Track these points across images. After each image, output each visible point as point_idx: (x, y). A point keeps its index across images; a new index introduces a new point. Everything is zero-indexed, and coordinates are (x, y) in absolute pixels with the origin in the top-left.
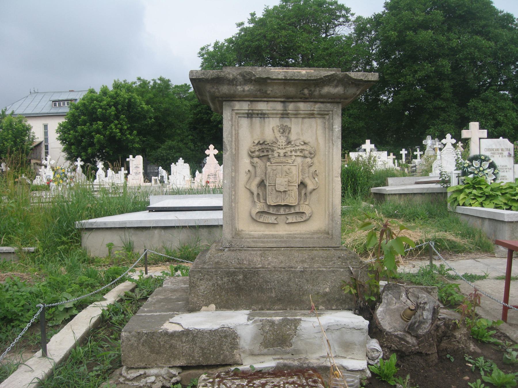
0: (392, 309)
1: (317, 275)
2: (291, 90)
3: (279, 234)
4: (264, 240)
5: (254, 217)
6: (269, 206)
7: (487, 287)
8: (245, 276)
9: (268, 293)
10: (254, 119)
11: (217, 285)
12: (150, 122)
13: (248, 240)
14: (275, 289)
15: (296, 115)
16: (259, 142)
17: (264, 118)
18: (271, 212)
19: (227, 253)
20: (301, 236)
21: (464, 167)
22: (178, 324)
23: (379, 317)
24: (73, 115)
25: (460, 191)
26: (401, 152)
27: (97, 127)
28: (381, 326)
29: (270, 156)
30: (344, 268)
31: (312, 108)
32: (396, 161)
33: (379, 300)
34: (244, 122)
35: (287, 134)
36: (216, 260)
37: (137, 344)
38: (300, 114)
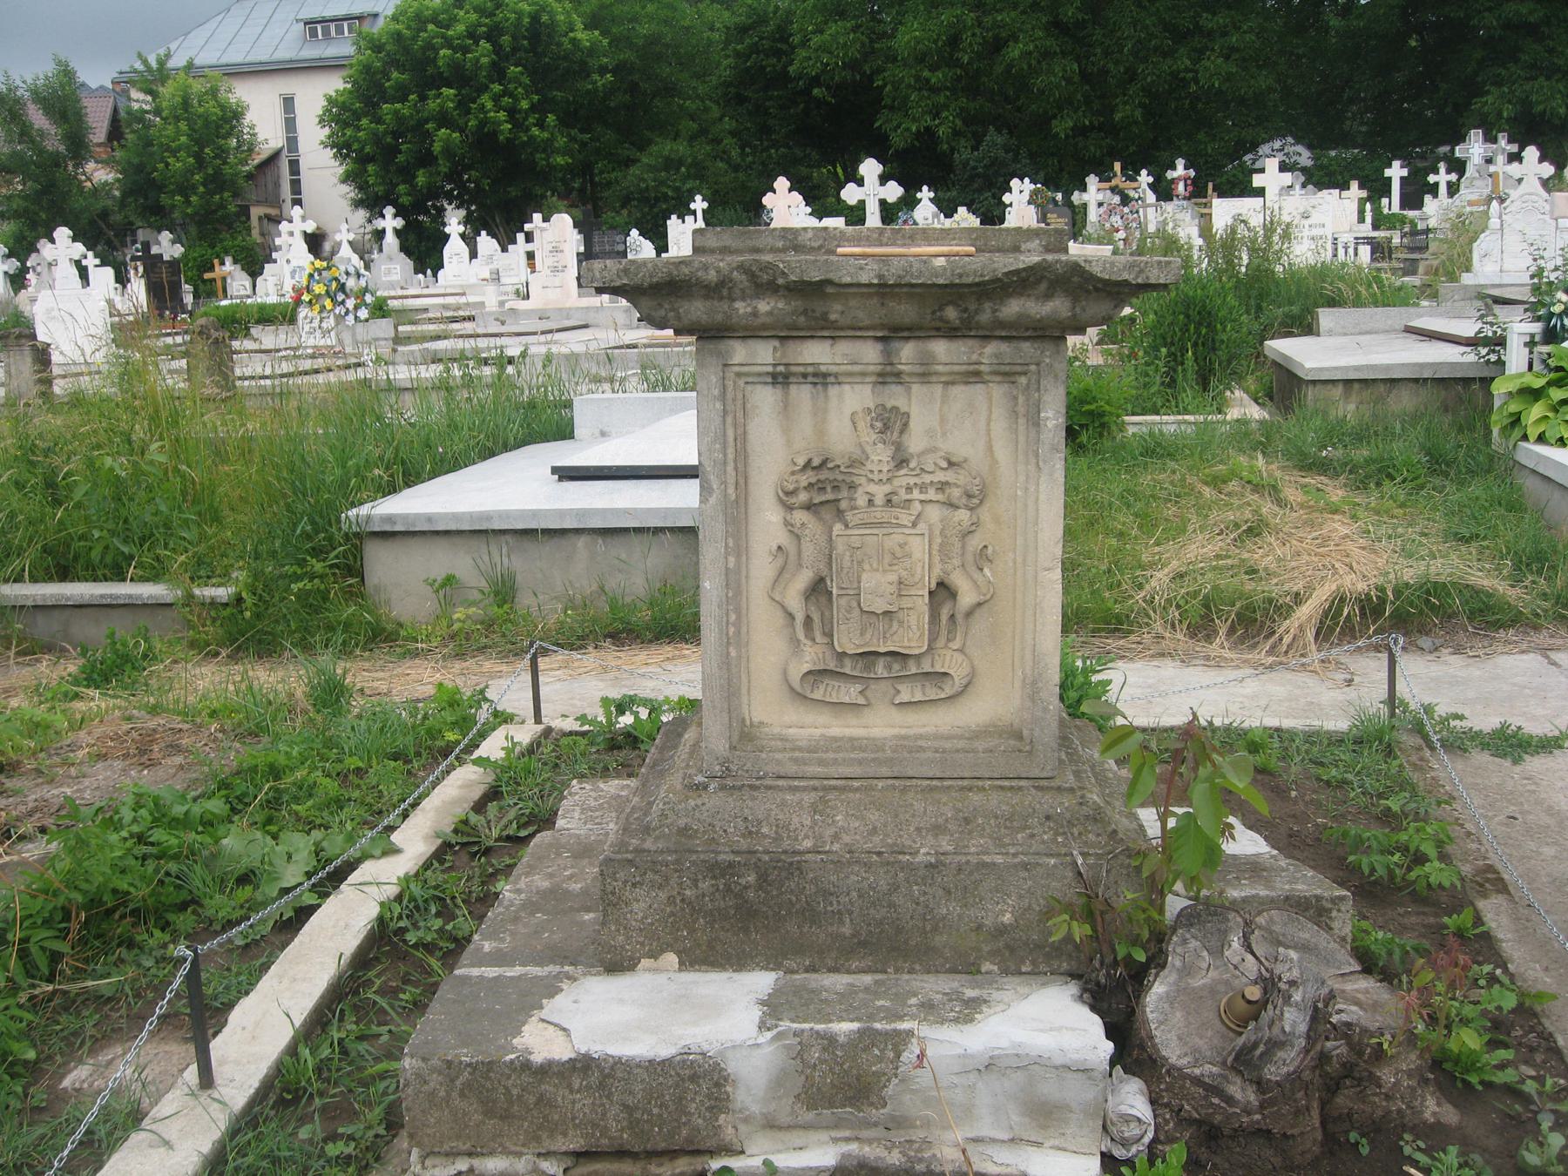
0: (1194, 989)
1: (976, 876)
2: (906, 312)
3: (872, 735)
4: (824, 756)
5: (797, 686)
6: (842, 656)
7: (1560, 784)
8: (763, 878)
9: (832, 924)
10: (793, 389)
11: (683, 900)
12: (599, 84)
13: (778, 756)
14: (850, 913)
15: (925, 377)
16: (810, 461)
17: (825, 385)
18: (847, 670)
19: (713, 800)
20: (936, 744)
21: (1552, 315)
22: (564, 1029)
23: (1150, 1016)
24: (367, 69)
25: (1533, 394)
26: (1388, 172)
27: (441, 106)
28: (1154, 1046)
29: (844, 505)
30: (1059, 855)
31: (974, 357)
32: (1368, 206)
33: (1157, 961)
34: (765, 398)
35: (896, 434)
36: (682, 822)
37: (446, 1091)
38: (936, 373)
